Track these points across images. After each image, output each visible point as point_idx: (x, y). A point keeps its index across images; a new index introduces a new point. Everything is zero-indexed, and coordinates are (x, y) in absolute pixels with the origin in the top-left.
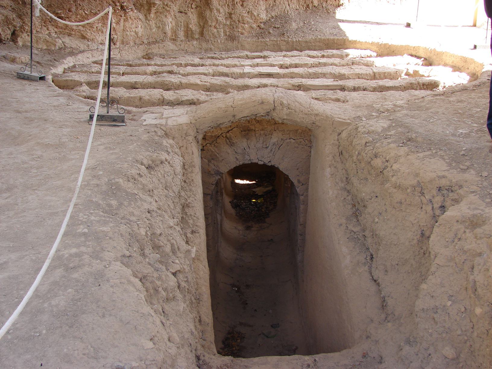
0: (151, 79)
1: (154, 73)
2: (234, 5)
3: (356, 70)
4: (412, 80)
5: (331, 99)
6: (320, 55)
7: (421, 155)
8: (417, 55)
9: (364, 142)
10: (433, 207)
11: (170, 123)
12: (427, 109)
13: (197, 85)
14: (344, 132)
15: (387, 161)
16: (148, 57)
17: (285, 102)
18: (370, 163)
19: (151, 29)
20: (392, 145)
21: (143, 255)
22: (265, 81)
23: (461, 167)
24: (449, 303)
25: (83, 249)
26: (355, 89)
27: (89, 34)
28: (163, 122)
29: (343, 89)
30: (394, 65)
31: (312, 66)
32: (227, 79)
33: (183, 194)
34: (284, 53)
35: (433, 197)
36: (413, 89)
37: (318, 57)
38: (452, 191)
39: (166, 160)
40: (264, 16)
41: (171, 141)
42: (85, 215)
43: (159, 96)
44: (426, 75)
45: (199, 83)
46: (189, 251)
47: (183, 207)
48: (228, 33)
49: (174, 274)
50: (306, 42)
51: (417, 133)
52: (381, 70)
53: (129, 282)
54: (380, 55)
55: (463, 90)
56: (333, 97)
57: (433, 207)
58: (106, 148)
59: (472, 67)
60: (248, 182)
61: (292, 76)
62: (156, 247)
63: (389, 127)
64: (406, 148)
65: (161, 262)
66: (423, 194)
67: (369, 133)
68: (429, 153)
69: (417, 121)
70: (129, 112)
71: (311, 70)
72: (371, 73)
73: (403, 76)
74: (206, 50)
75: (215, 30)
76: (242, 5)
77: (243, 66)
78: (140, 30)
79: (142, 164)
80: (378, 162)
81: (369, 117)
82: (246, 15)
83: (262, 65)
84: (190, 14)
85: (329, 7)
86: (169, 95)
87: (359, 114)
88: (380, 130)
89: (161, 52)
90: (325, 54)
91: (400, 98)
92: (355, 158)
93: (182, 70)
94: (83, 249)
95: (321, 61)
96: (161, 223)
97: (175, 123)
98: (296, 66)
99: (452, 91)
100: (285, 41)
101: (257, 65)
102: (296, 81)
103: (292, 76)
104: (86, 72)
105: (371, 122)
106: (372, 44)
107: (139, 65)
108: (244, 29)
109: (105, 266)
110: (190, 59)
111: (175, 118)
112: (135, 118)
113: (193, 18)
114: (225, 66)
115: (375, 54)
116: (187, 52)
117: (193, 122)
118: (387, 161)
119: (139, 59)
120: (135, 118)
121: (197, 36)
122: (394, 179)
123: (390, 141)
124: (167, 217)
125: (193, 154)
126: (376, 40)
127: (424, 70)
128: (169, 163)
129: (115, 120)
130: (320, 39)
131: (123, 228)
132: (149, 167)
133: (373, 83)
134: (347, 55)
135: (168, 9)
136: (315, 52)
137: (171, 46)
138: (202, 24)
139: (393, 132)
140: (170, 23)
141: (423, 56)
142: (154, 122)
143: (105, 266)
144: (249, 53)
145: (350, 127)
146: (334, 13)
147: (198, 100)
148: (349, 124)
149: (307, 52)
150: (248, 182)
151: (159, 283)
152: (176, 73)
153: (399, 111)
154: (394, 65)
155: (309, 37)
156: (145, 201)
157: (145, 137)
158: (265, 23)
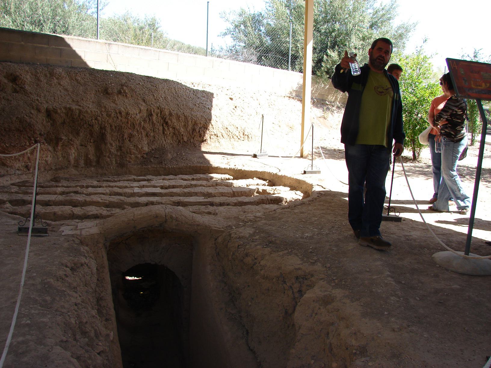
0: (61, 198)
1: (62, 193)
2: (123, 140)
3: (220, 190)
4: (263, 197)
5: (204, 212)
6: (191, 178)
7: (281, 253)
8: (264, 178)
9: (237, 245)
10: (293, 292)
11: (84, 233)
12: (280, 219)
13: (99, 202)
14: (220, 238)
15: (256, 259)
16: (56, 180)
17: (174, 216)
18: (242, 261)
19: (58, 158)
20: (259, 247)
21: (75, 339)
22: (152, 199)
23: (311, 261)
24: (312, 362)
25: (28, 337)
26: (221, 204)
27: (8, 162)
28: (78, 232)
29: (212, 204)
30: (247, 186)
31: (186, 187)
32: (122, 198)
33: (97, 289)
34: (163, 177)
35: (293, 284)
36: (264, 203)
37: (189, 180)
38: (306, 279)
39: (85, 263)
40: (146, 149)
41: (86, 248)
42: (26, 309)
43: (69, 212)
44: (272, 192)
45: (101, 201)
46: (108, 335)
47: (98, 300)
48: (118, 162)
49: (99, 354)
50: (179, 168)
51: (275, 237)
52: (238, 190)
53: (70, 362)
54: (236, 178)
55: (302, 204)
56: (206, 211)
57: (293, 292)
58: (36, 254)
59: (304, 187)
60: (136, 278)
61: (172, 195)
62: (84, 333)
63: (255, 232)
64: (269, 249)
65: (88, 345)
66: (285, 282)
67: (239, 238)
68: (286, 252)
69: (274, 228)
70: (49, 225)
71: (186, 190)
72: (231, 192)
73: (256, 194)
74: (101, 175)
75: (109, 159)
76: (130, 141)
77: (132, 187)
78: (49, 159)
79: (67, 266)
80: (248, 260)
81: (238, 226)
82: (132, 148)
83: (147, 187)
84: (89, 147)
85: (196, 142)
86: (77, 211)
87: (230, 223)
88: (248, 236)
89: (65, 176)
90: (195, 178)
91: (258, 211)
92: (230, 257)
93: (85, 191)
94: (28, 337)
95: (192, 183)
96: (86, 313)
97: (88, 234)
98: (174, 187)
99: (294, 204)
100: (163, 167)
101: (143, 186)
102: (176, 199)
103: (172, 195)
104: (7, 192)
105: (241, 230)
106: (230, 169)
107: (50, 187)
108: (131, 158)
109: (48, 350)
110: (89, 182)
111: (87, 230)
112: (54, 229)
113: (91, 149)
114: (118, 187)
115: (232, 178)
116: (86, 176)
117: (103, 232)
118: (256, 259)
119: (49, 182)
120: (54, 229)
121: (94, 164)
122: (262, 272)
123: (256, 243)
124: (90, 309)
125: (103, 257)
126: (232, 167)
127: (269, 189)
128: (87, 265)
129: (39, 232)
130: (190, 166)
131: (59, 318)
132: (72, 269)
133: (234, 200)
134: (212, 178)
135: (72, 143)
136: (187, 176)
137: (74, 171)
138: (98, 154)
139: (257, 237)
140: (73, 153)
141: (267, 178)
142: (70, 233)
143: (48, 350)
144: (135, 177)
145: (224, 234)
146: (200, 147)
147: (101, 214)
148: (223, 232)
149: (180, 176)
150: (136, 278)
151: (90, 362)
152: (80, 193)
153: (259, 221)
154: (247, 186)
155: (182, 165)
156: (73, 296)
157: (66, 245)
158: (147, 154)
